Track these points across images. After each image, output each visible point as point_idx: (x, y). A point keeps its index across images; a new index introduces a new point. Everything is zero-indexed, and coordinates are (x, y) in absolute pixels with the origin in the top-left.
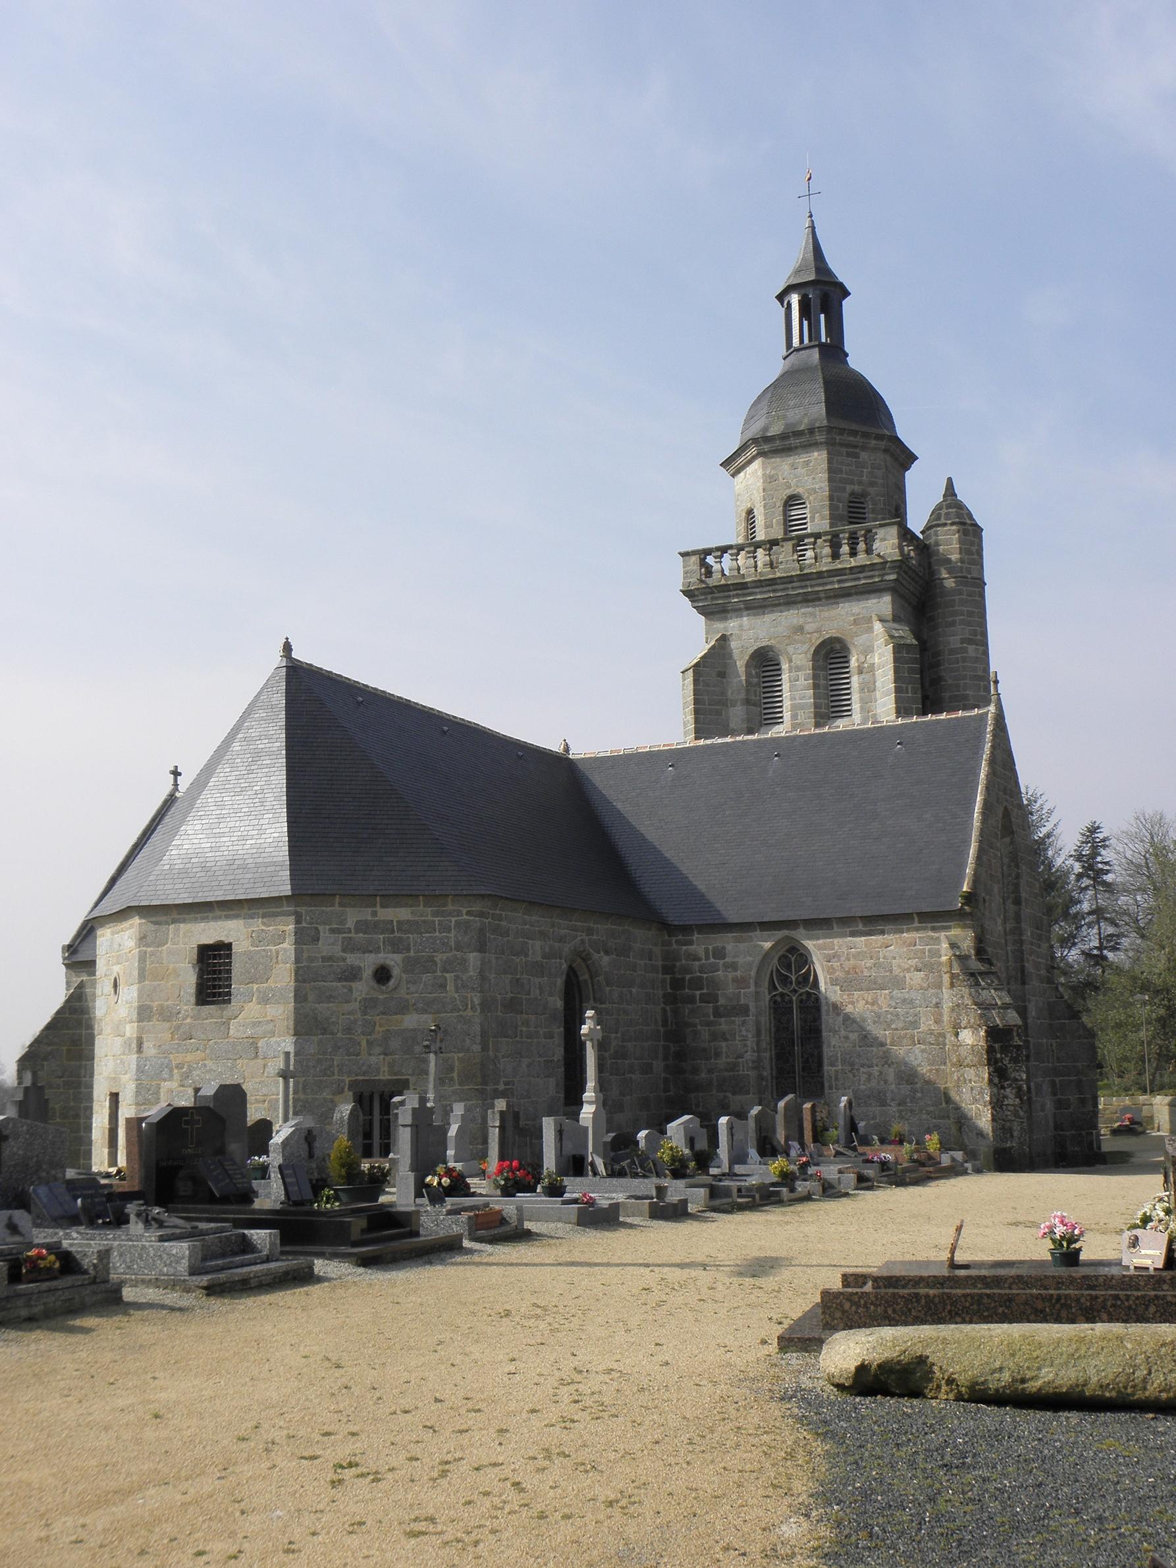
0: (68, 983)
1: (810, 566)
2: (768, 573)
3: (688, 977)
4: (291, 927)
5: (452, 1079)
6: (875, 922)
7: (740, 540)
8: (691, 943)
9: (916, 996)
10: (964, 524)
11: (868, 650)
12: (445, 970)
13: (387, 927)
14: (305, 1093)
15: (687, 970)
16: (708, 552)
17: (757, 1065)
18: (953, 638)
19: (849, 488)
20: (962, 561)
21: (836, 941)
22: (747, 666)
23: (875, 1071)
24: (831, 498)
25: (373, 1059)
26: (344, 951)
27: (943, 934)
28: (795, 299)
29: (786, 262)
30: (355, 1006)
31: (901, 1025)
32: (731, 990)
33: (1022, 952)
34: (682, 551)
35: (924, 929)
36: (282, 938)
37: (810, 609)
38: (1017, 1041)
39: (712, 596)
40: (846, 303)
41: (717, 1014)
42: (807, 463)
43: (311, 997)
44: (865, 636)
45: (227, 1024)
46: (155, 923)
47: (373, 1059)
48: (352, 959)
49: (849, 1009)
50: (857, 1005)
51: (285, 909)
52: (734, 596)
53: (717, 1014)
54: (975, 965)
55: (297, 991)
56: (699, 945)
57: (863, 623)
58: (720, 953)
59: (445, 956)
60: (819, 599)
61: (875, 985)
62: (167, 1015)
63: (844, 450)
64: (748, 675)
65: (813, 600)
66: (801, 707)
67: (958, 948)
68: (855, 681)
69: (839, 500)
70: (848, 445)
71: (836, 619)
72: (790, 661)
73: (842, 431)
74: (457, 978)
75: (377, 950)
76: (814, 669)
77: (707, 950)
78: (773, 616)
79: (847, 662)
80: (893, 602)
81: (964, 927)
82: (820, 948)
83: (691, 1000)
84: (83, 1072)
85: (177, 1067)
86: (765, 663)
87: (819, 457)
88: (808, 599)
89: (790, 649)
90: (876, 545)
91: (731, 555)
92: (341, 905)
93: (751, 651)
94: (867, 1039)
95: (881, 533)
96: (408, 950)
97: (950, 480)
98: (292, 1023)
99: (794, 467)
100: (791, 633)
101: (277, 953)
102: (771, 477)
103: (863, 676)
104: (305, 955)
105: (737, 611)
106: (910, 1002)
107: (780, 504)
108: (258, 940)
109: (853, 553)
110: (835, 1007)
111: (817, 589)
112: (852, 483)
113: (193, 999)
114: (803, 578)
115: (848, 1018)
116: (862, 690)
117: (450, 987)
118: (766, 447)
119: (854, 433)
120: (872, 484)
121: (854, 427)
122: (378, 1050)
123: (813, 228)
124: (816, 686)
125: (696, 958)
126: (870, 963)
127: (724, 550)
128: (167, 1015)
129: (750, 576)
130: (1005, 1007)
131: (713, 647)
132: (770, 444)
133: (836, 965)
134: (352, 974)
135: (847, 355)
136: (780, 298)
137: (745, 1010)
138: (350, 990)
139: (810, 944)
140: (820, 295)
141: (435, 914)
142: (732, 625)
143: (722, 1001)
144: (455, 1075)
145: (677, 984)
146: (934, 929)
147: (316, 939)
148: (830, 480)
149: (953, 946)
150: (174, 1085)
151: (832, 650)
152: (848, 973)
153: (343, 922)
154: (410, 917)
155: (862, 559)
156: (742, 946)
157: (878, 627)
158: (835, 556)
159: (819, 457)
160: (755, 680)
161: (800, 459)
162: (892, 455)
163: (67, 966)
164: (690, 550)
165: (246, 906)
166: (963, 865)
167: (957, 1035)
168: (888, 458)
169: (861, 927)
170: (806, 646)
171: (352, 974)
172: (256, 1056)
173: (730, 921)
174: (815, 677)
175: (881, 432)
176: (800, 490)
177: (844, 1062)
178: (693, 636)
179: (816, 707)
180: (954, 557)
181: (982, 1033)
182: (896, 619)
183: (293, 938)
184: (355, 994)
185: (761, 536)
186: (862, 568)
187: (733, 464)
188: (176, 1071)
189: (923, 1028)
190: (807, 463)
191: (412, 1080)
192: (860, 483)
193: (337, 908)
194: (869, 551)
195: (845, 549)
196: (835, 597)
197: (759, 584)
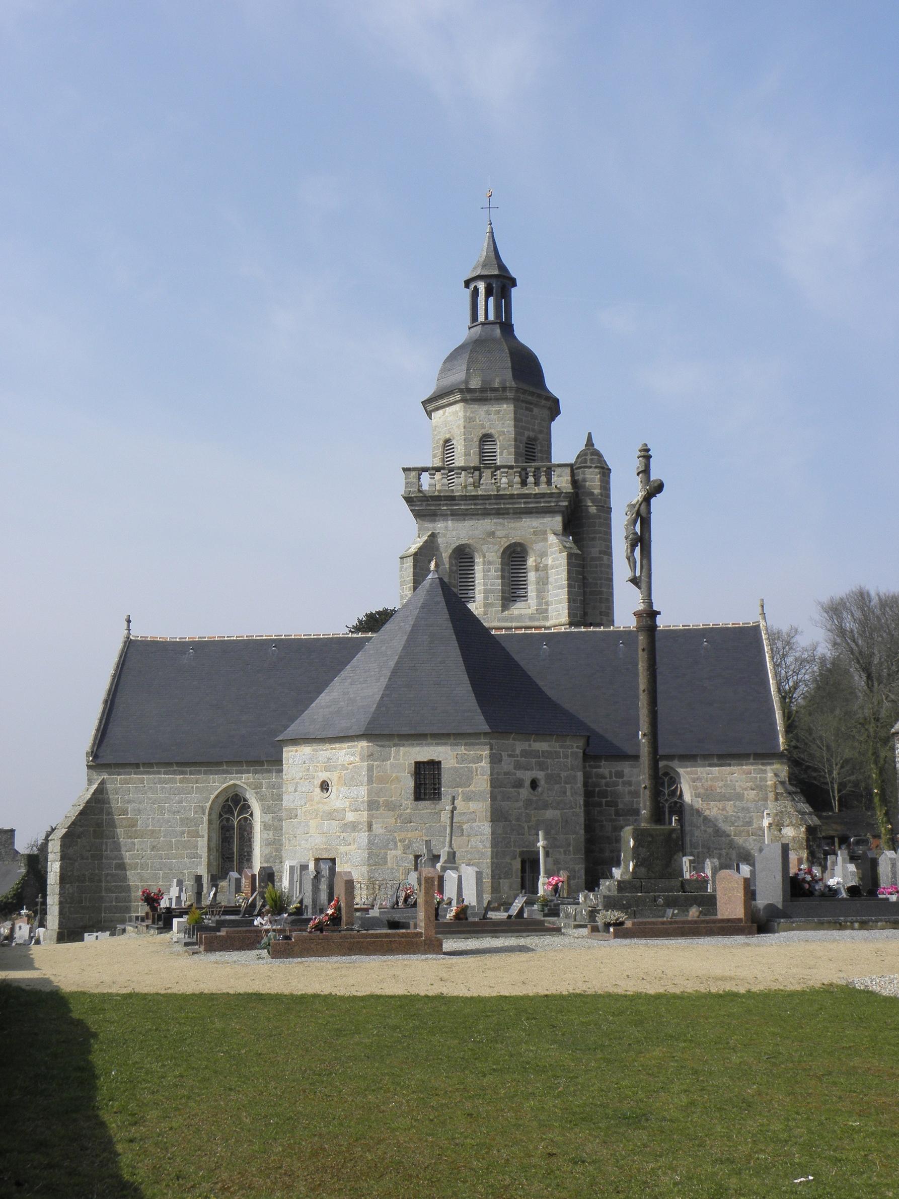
0: (90, 782)
1: (505, 489)
2: (472, 491)
3: (597, 789)
4: (487, 752)
5: (569, 851)
6: (726, 757)
7: (438, 463)
8: (599, 767)
9: (751, 805)
10: (603, 468)
12: (566, 783)
14: (497, 858)
19: (527, 433)
20: (601, 495)
21: (699, 769)
22: (450, 557)
23: (724, 852)
24: (516, 440)
26: (515, 769)
27: (768, 768)
28: (482, 286)
29: (473, 259)
30: (521, 804)
31: (741, 823)
32: (627, 798)
34: (405, 467)
36: (479, 759)
37: (501, 520)
39: (424, 506)
40: (514, 291)
41: (617, 814)
43: (499, 798)
44: (541, 544)
46: (381, 746)
48: (520, 774)
49: (707, 813)
50: (712, 810)
51: (482, 740)
52: (444, 505)
53: (617, 814)
55: (492, 792)
57: (541, 534)
58: (620, 775)
60: (508, 514)
61: (724, 798)
62: (391, 807)
63: (524, 405)
64: (451, 564)
65: (503, 514)
66: (492, 591)
68: (532, 576)
69: (520, 442)
70: (527, 402)
71: (522, 529)
72: (484, 557)
73: (525, 392)
74: (572, 788)
75: (532, 769)
76: (502, 564)
77: (610, 772)
78: (472, 523)
79: (525, 561)
81: (782, 763)
82: (688, 773)
84: (104, 847)
85: (400, 841)
86: (463, 557)
87: (507, 409)
89: (485, 548)
90: (554, 479)
91: (443, 474)
92: (513, 739)
93: (454, 546)
94: (718, 832)
96: (547, 769)
97: (590, 434)
98: (489, 814)
99: (488, 413)
100: (485, 537)
101: (477, 768)
102: (470, 418)
103: (540, 573)
104: (496, 771)
105: (444, 516)
106: (747, 810)
107: (476, 440)
108: (461, 759)
109: (537, 483)
110: (698, 811)
111: (508, 506)
112: (528, 430)
113: (412, 797)
114: (499, 497)
115: (706, 819)
116: (538, 583)
117: (568, 793)
118: (468, 396)
121: (532, 389)
123: (492, 233)
124: (503, 577)
125: (603, 777)
126: (721, 784)
128: (391, 807)
129: (458, 491)
130: (810, 814)
131: (426, 542)
133: (699, 784)
134: (519, 784)
136: (467, 284)
138: (519, 793)
139: (681, 771)
140: (500, 284)
141: (561, 747)
142: (440, 526)
143: (621, 806)
144: (571, 848)
146: (763, 764)
147: (500, 761)
148: (516, 426)
149: (776, 775)
150: (399, 852)
151: (514, 552)
152: (707, 790)
153: (514, 750)
154: (548, 749)
155: (543, 488)
157: (552, 539)
158: (524, 483)
159: (507, 409)
160: (455, 568)
161: (494, 408)
163: (89, 767)
164: (411, 466)
165: (452, 738)
166: (773, 724)
167: (780, 830)
169: (715, 761)
170: (497, 547)
171: (519, 784)
172: (462, 835)
173: (630, 754)
176: (492, 431)
177: (703, 846)
178: (410, 535)
179: (503, 592)
180: (597, 491)
181: (803, 829)
183: (488, 760)
184: (521, 796)
185: (459, 462)
186: (543, 495)
187: (432, 404)
188: (399, 844)
190: (498, 412)
194: (549, 482)
195: (531, 479)
196: (521, 513)
197: (465, 498)
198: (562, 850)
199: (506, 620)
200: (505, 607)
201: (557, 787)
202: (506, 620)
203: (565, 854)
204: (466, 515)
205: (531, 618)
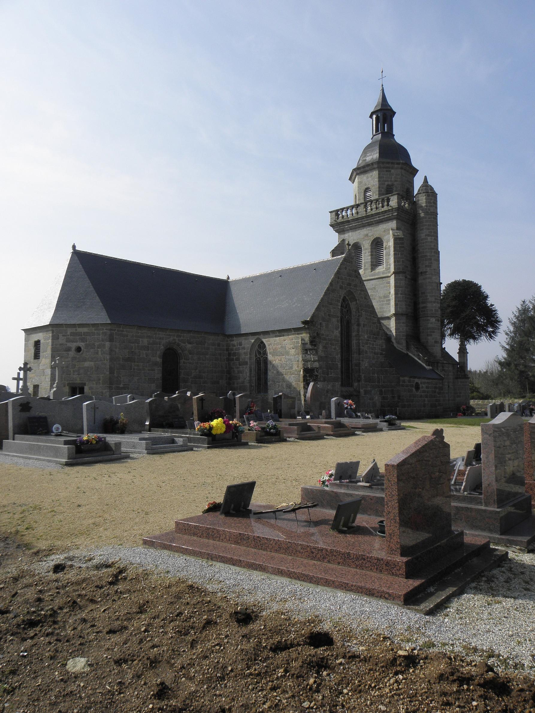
1: (369, 212)
4: (51, 335)
10: (428, 192)
11: (388, 241)
13: (80, 334)
15: (232, 350)
16: (338, 211)
17: (250, 381)
18: (422, 234)
19: (386, 183)
20: (426, 206)
24: (379, 187)
25: (75, 376)
28: (374, 116)
29: (373, 103)
30: (70, 359)
31: (288, 368)
33: (359, 343)
35: (295, 334)
38: (316, 373)
42: (372, 176)
45: (39, 365)
47: (75, 376)
48: (69, 344)
49: (274, 362)
53: (240, 365)
54: (309, 346)
56: (235, 341)
58: (240, 344)
59: (98, 343)
63: (385, 169)
66: (367, 262)
67: (304, 340)
69: (382, 188)
73: (383, 163)
75: (77, 342)
78: (359, 231)
80: (397, 223)
83: (233, 360)
86: (357, 247)
87: (375, 174)
88: (370, 224)
94: (279, 373)
95: (392, 198)
97: (426, 177)
102: (360, 182)
107: (363, 191)
112: (388, 181)
113: (33, 357)
114: (367, 217)
117: (100, 353)
118: (358, 172)
119: (388, 163)
120: (396, 181)
121: (389, 161)
122: (76, 373)
123: (383, 90)
124: (372, 255)
127: (347, 208)
130: (314, 361)
132: (360, 170)
134: (69, 349)
135: (394, 135)
137: (246, 363)
138: (68, 354)
139: (264, 340)
140: (384, 115)
145: (229, 354)
148: (379, 181)
153: (66, 333)
155: (386, 208)
156: (246, 341)
159: (375, 174)
161: (369, 175)
162: (405, 170)
164: (332, 210)
168: (403, 171)
171: (69, 349)
174: (372, 252)
175: (399, 162)
176: (369, 186)
178: (333, 239)
180: (424, 205)
182: (397, 229)
186: (385, 212)
189: (294, 369)
190: (372, 176)
191: (87, 383)
192: (391, 181)
193: (65, 328)
194: (388, 205)
197: (354, 220)
198: (94, 382)
199: (375, 275)
200: (373, 269)
201: (92, 350)
202: (375, 275)
203: (97, 384)
204: (356, 228)
205: (383, 273)
